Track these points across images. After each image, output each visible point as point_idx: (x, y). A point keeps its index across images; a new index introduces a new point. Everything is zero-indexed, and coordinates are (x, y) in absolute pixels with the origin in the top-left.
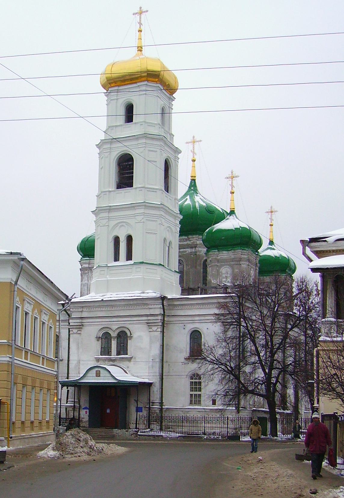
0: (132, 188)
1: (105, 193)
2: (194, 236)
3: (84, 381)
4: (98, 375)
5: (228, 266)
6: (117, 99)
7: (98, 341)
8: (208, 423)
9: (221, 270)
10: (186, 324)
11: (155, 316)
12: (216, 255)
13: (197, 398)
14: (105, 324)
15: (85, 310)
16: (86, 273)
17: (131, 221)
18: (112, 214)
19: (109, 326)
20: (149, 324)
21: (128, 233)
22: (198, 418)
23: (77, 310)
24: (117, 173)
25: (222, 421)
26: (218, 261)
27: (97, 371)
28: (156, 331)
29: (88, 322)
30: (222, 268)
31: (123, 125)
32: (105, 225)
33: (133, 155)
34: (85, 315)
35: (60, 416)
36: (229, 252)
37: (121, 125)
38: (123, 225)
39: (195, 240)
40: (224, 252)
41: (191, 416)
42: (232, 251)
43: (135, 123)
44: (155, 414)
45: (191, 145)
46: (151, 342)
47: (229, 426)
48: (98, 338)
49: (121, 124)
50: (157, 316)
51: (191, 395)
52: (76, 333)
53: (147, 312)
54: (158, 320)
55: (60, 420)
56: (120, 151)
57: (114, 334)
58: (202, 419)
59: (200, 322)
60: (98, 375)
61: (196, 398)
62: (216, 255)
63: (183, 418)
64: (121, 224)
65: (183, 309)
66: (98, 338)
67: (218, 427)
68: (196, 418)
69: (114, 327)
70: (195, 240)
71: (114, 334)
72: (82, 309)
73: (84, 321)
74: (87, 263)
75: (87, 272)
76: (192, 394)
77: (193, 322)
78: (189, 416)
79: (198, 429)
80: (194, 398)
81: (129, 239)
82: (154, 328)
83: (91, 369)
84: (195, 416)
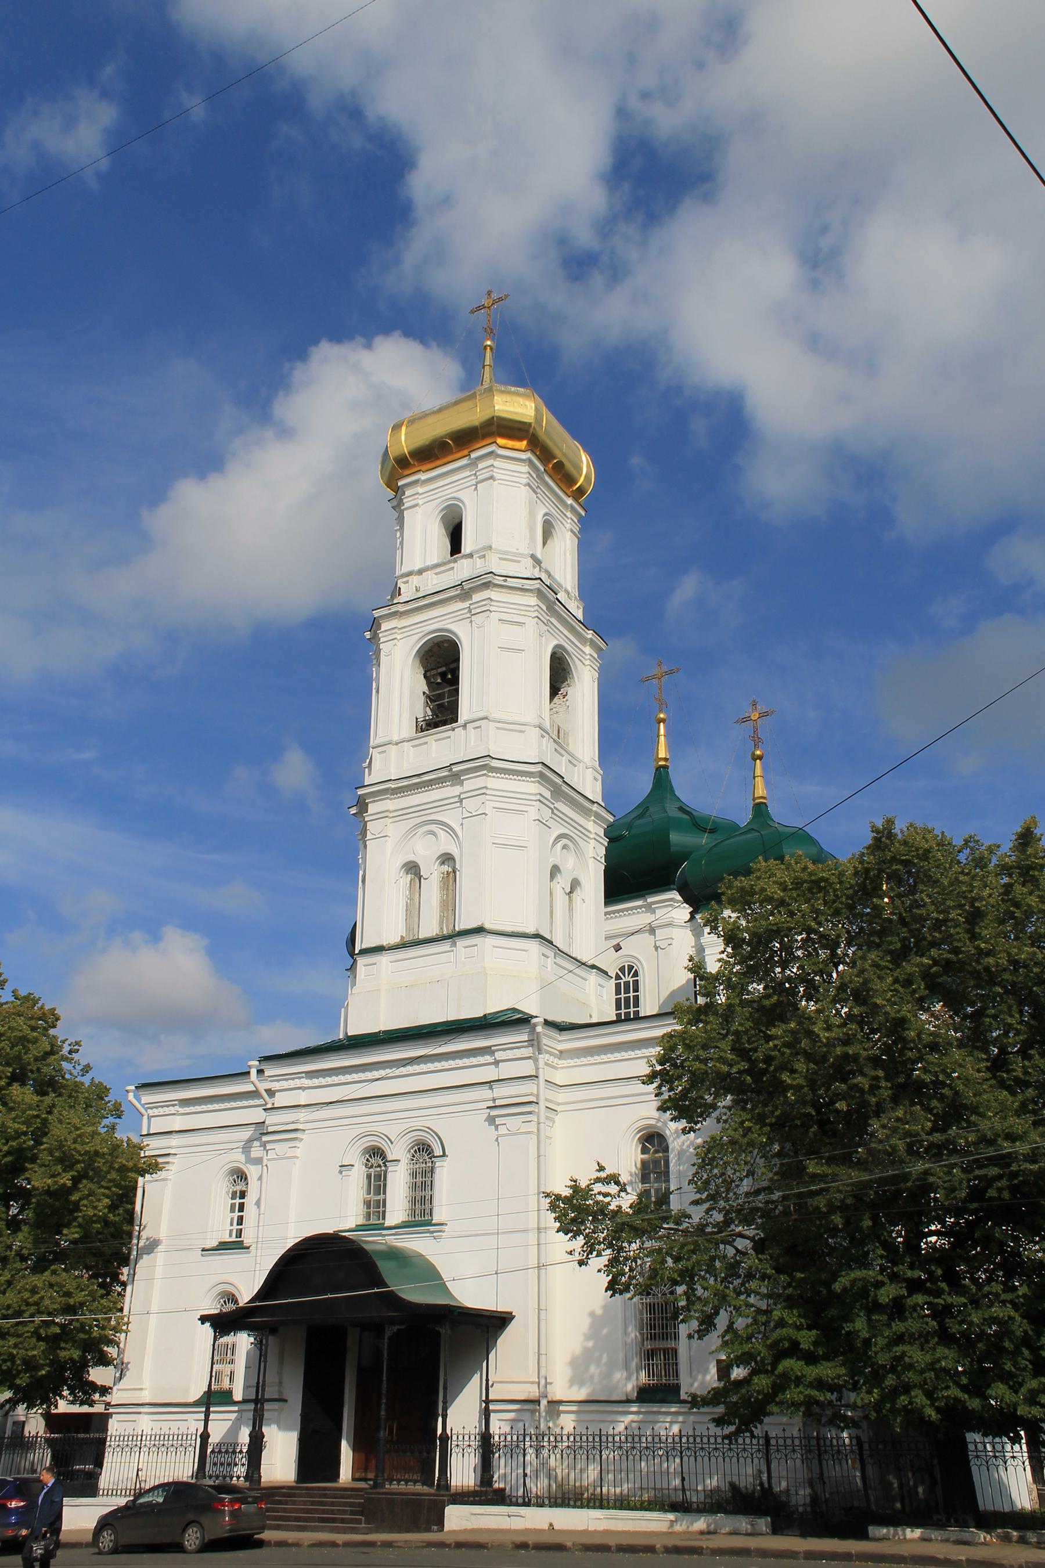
43: (470, 556)
53: (490, 1073)
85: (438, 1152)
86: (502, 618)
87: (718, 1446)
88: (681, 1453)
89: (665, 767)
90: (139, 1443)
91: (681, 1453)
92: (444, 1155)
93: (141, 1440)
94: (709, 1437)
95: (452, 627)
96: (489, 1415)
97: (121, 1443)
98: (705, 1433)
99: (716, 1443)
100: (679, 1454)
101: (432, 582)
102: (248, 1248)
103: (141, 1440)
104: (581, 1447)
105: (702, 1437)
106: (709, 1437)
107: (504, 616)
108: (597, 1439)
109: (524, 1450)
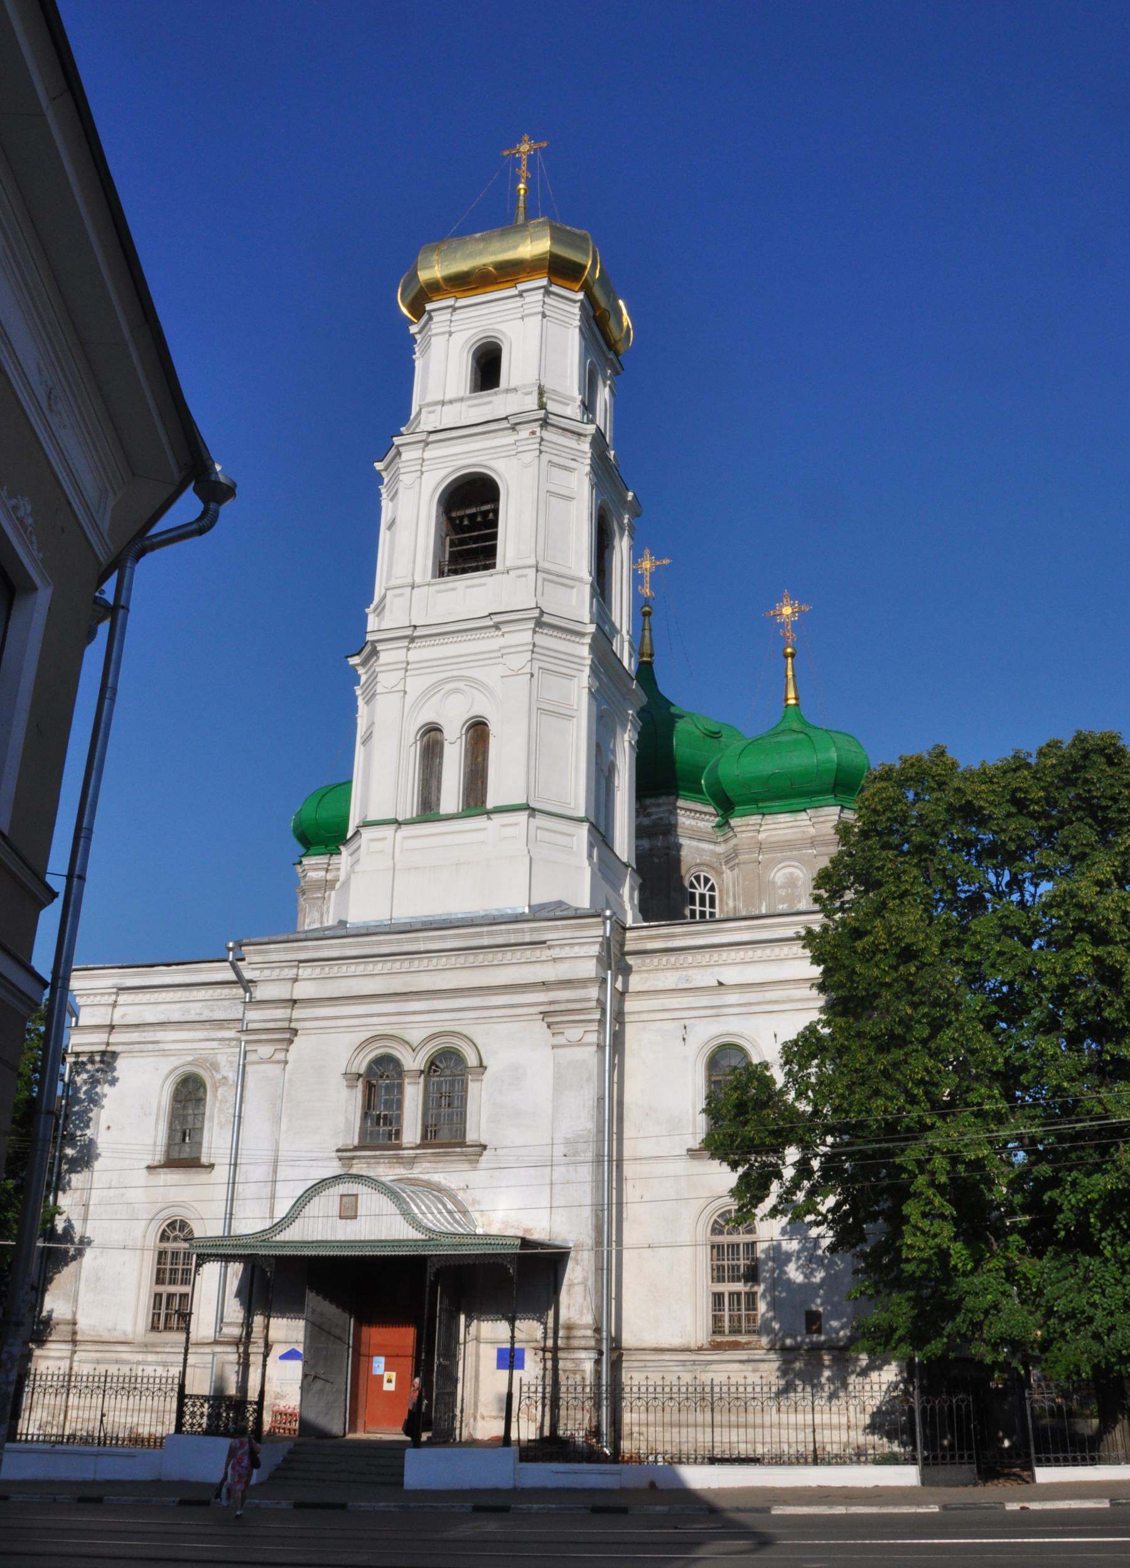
0: (491, 571)
1: (398, 591)
2: (661, 800)
3: (291, 1234)
4: (348, 1211)
5: (796, 864)
6: (450, 334)
7: (351, 1087)
8: (792, 1409)
9: (773, 874)
10: (693, 1021)
11: (576, 988)
12: (753, 828)
13: (739, 1310)
14: (380, 1026)
15: (305, 972)
16: (317, 898)
17: (490, 675)
18: (418, 653)
19: (399, 1031)
20: (550, 1017)
21: (475, 714)
22: (750, 1389)
23: (275, 974)
24: (365, 922)
25: (704, 1399)
26: (760, 847)
27: (345, 1199)
28: (579, 1043)
29: (317, 1019)
30: (776, 869)
31: (469, 399)
32: (394, 690)
33: (501, 478)
34: (302, 991)
35: (182, 1386)
36: (799, 818)
37: (462, 400)
38: (456, 691)
39: (664, 812)
40: (782, 818)
41: (651, 1382)
42: (808, 811)
43: (507, 391)
44: (578, 1378)
45: (278, 1396)
46: (560, 1083)
47: (717, 1418)
48: (352, 1078)
49: (461, 394)
50: (585, 987)
51: (718, 1298)
52: (269, 1060)
53: (549, 973)
54: (588, 1000)
55: (181, 1405)
56: (454, 468)
57: (413, 1062)
58: (698, 1395)
59: (747, 1010)
60: (348, 1211)
61: (736, 1307)
62: (753, 828)
63: (717, 1389)
64: (448, 687)
65: (678, 968)
66: (352, 1078)
67: (754, 1427)
68: (741, 1389)
69: (416, 1035)
70: (664, 812)
71: (413, 1062)
72: (295, 971)
73: (297, 1013)
74: (320, 866)
75: (319, 895)
76: (723, 1294)
77: (717, 1012)
78: (675, 1382)
79: (768, 1439)
80: (730, 1310)
81: (478, 731)
82: (574, 1033)
83: (323, 1184)
84: (671, 1378)
85: (472, 1060)
86: (553, 460)
87: (756, 1395)
88: (104, 1391)
89: (650, 664)
90: (102, 1385)
91: (104, 1391)
92: (482, 1066)
93: (105, 1381)
94: (762, 1386)
95: (493, 464)
96: (359, 1360)
97: (126, 1385)
98: (741, 1381)
99: (148, 1383)
100: (810, 1404)
101: (449, 417)
102: (211, 1166)
103: (105, 1381)
104: (160, 1389)
105: (53, 1375)
106: (167, 1379)
107: (556, 459)
108: (103, 1379)
109: (712, 1404)
